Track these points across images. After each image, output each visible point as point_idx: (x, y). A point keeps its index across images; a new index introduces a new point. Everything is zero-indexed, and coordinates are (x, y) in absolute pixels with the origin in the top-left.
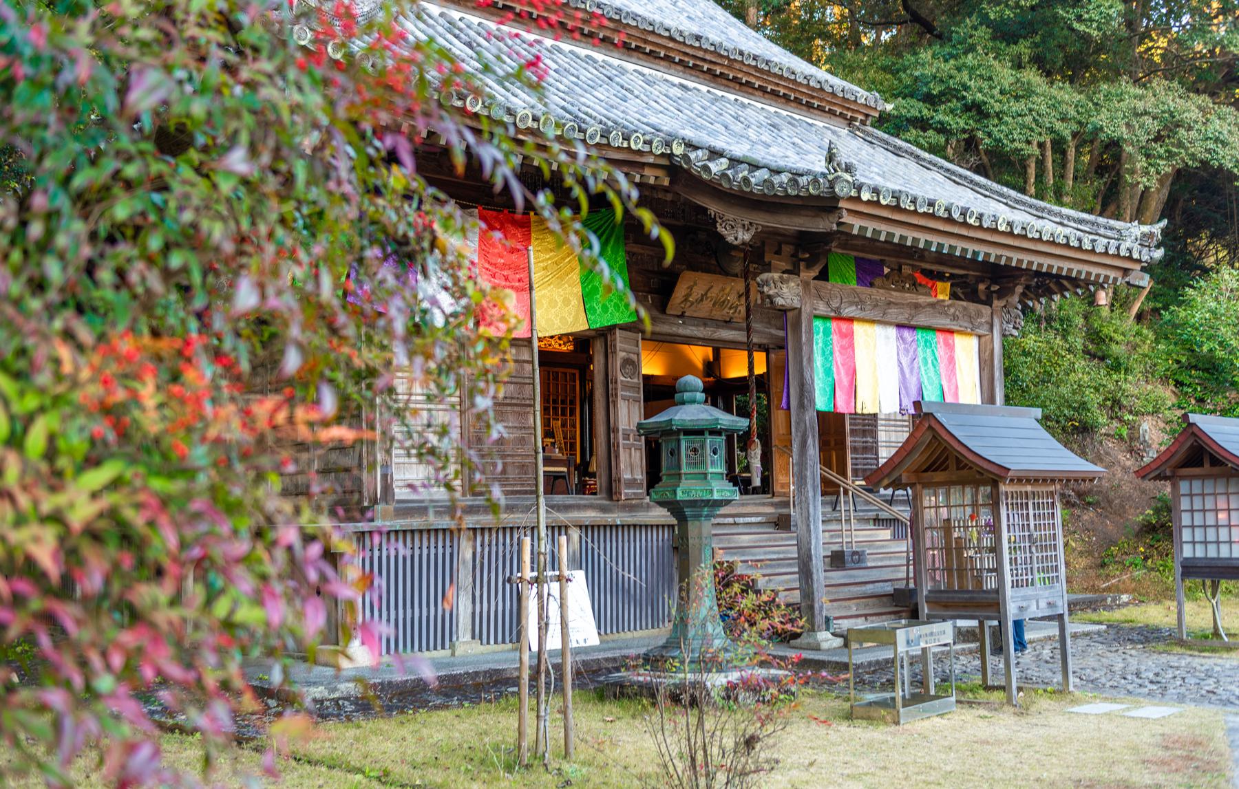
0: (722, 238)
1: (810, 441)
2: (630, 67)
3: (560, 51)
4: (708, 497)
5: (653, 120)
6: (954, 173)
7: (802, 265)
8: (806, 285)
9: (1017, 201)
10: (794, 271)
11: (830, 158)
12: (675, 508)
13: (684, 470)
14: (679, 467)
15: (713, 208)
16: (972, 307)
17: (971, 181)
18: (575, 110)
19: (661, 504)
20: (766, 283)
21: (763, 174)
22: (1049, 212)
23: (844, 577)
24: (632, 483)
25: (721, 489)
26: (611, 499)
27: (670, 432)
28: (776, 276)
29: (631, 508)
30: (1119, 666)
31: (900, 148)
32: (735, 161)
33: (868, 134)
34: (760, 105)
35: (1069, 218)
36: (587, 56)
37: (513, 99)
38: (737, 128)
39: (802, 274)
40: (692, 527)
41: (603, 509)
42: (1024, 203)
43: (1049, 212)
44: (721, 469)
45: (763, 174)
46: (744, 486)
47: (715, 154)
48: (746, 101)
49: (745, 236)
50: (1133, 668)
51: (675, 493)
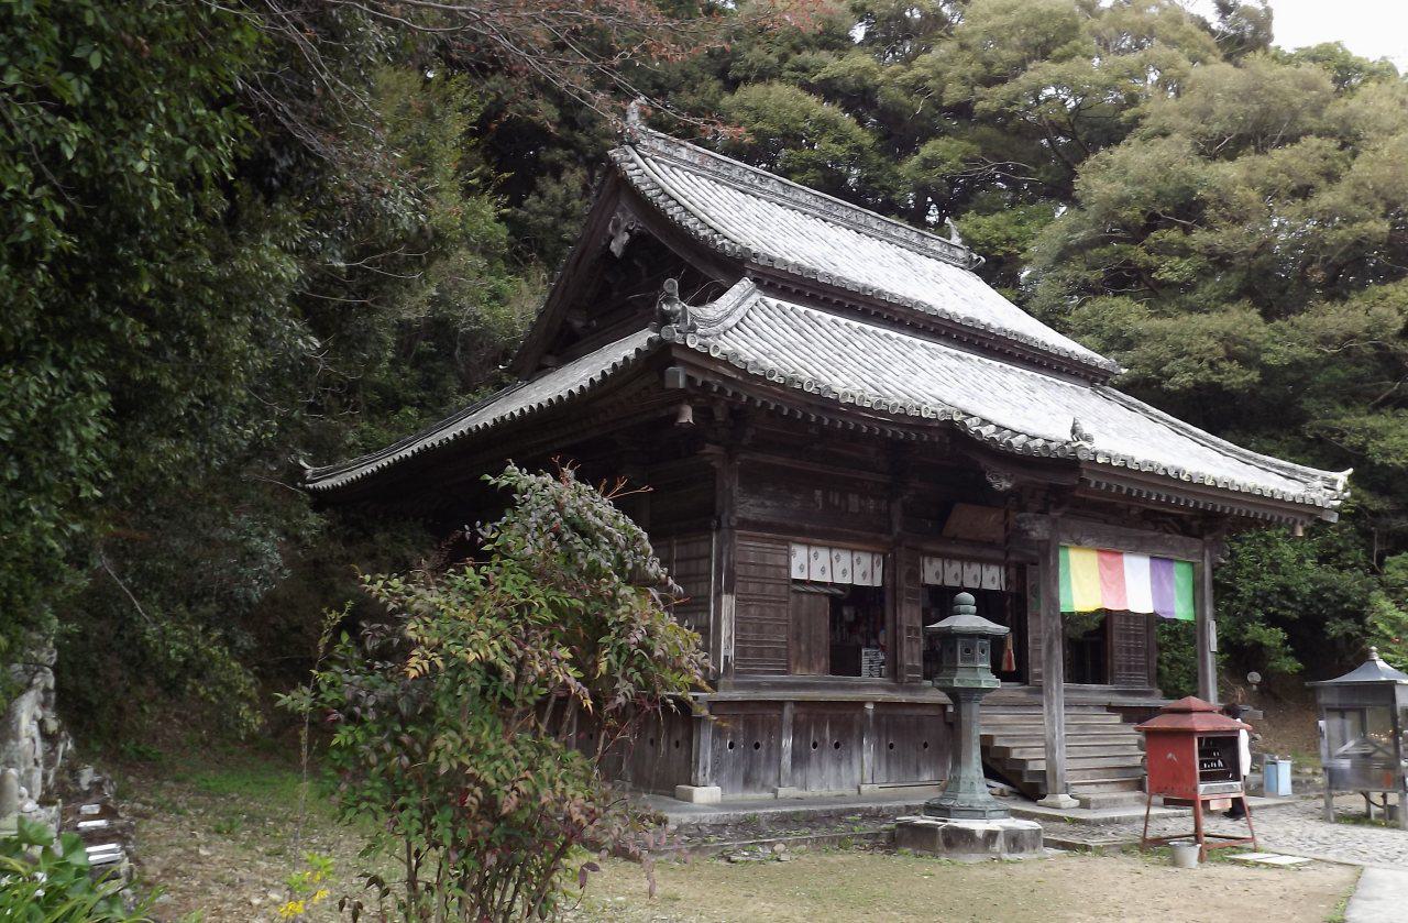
0: (991, 485)
1: (1056, 643)
2: (918, 342)
3: (863, 331)
4: (977, 686)
5: (937, 391)
6: (1177, 426)
7: (1051, 506)
8: (1054, 521)
9: (1228, 450)
10: (1044, 512)
11: (1074, 431)
12: (954, 694)
13: (960, 664)
14: (956, 662)
15: (984, 463)
16: (1187, 540)
17: (1191, 433)
18: (879, 386)
19: (942, 689)
20: (1022, 520)
21: (1022, 438)
22: (1255, 460)
23: (1288, 486)
24: (913, 669)
25: (988, 680)
26: (895, 681)
27: (951, 636)
28: (1030, 515)
29: (911, 689)
30: (1296, 833)
31: (1133, 405)
32: (1000, 428)
33: (1106, 392)
34: (1019, 370)
35: (1271, 464)
36: (886, 335)
37: (834, 378)
38: (1001, 393)
39: (1051, 514)
40: (965, 709)
41: (889, 689)
42: (1231, 451)
43: (1255, 460)
44: (987, 665)
45: (1022, 438)
46: (1005, 676)
47: (985, 422)
48: (1008, 367)
49: (1006, 485)
50: (1307, 834)
51: (952, 681)
